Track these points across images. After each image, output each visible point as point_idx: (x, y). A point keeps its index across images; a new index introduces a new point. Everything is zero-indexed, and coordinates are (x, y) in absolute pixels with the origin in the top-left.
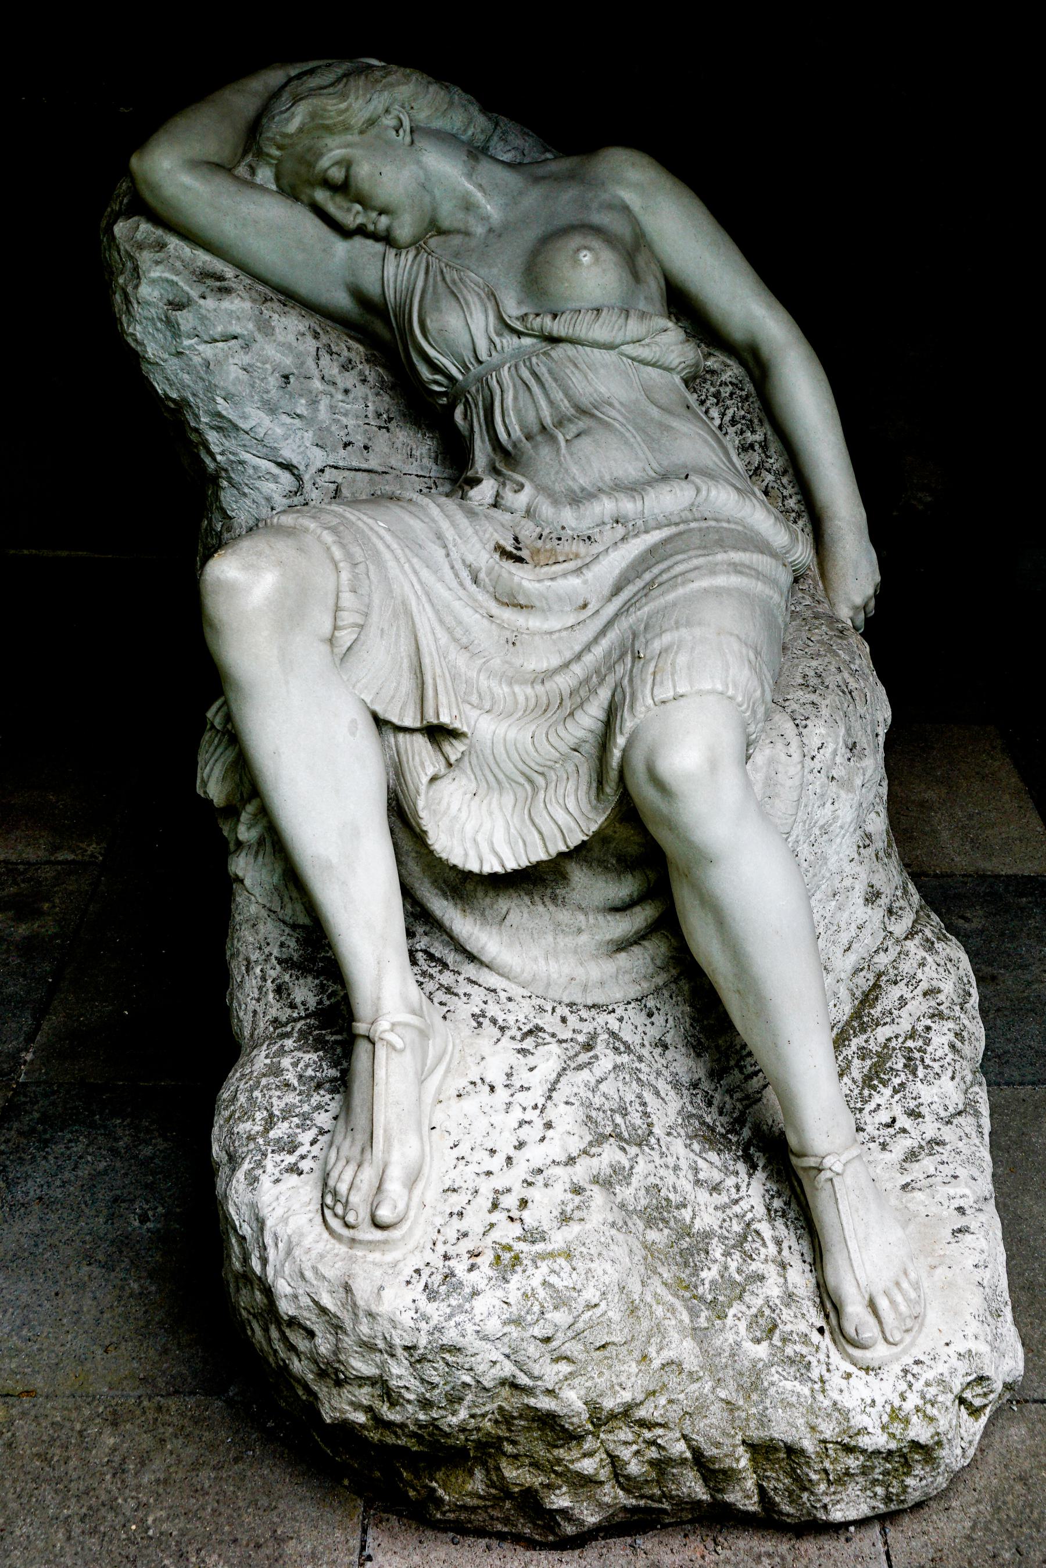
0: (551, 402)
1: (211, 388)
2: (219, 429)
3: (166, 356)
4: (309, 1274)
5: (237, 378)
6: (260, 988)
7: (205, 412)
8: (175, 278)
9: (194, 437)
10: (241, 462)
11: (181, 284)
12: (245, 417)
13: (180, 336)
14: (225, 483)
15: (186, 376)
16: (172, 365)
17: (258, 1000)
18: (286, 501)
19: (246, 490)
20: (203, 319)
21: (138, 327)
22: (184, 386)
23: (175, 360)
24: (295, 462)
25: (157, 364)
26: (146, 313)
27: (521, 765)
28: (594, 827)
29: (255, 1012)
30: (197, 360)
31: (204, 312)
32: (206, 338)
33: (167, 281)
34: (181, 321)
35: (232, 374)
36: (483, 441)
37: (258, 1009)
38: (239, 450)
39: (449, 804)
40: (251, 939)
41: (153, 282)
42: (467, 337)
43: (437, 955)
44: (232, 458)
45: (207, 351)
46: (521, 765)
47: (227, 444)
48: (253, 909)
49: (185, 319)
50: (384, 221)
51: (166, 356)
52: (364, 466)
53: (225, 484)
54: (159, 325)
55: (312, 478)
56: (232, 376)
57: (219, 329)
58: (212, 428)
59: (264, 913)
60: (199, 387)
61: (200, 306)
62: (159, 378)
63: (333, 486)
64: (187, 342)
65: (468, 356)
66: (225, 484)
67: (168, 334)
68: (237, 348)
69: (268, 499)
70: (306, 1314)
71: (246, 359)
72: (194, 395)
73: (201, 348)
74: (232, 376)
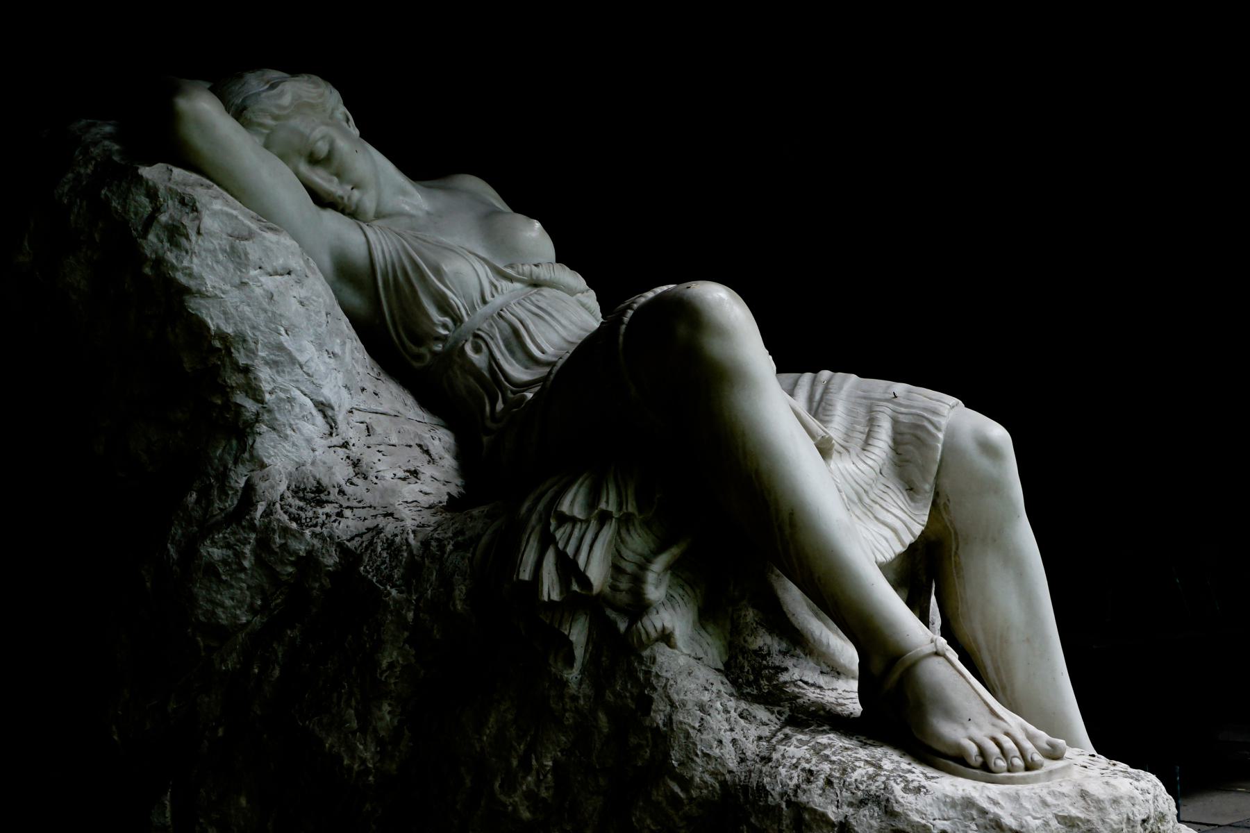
0: (564, 327)
1: (274, 318)
2: (273, 364)
3: (228, 287)
4: (1049, 799)
5: (297, 310)
6: (728, 720)
7: (265, 345)
8: (235, 213)
9: (234, 379)
10: (290, 400)
11: (240, 217)
12: (301, 351)
13: (246, 266)
14: (263, 428)
15: (247, 309)
16: (233, 297)
17: (732, 730)
18: (324, 442)
19: (289, 432)
20: (266, 250)
21: (195, 260)
22: (243, 318)
23: (236, 292)
24: (332, 402)
25: (216, 296)
26: (208, 245)
27: (857, 487)
29: (734, 741)
30: (258, 291)
31: (268, 244)
32: (270, 270)
33: (227, 214)
34: (248, 250)
36: (511, 364)
37: (736, 737)
38: (291, 386)
39: (647, 633)
40: (693, 686)
41: (215, 214)
42: (476, 279)
43: (811, 681)
44: (282, 395)
45: (269, 282)
46: (854, 484)
47: (279, 379)
48: (682, 660)
49: (253, 250)
51: (228, 287)
52: (381, 409)
53: (263, 428)
54: (221, 256)
55: (346, 418)
56: (294, 308)
57: (281, 261)
58: (267, 363)
59: (692, 661)
60: (261, 320)
61: (264, 238)
63: (364, 426)
64: (253, 273)
66: (263, 428)
67: (231, 266)
68: (292, 282)
69: (309, 441)
71: (303, 293)
72: (253, 328)
74: (294, 308)
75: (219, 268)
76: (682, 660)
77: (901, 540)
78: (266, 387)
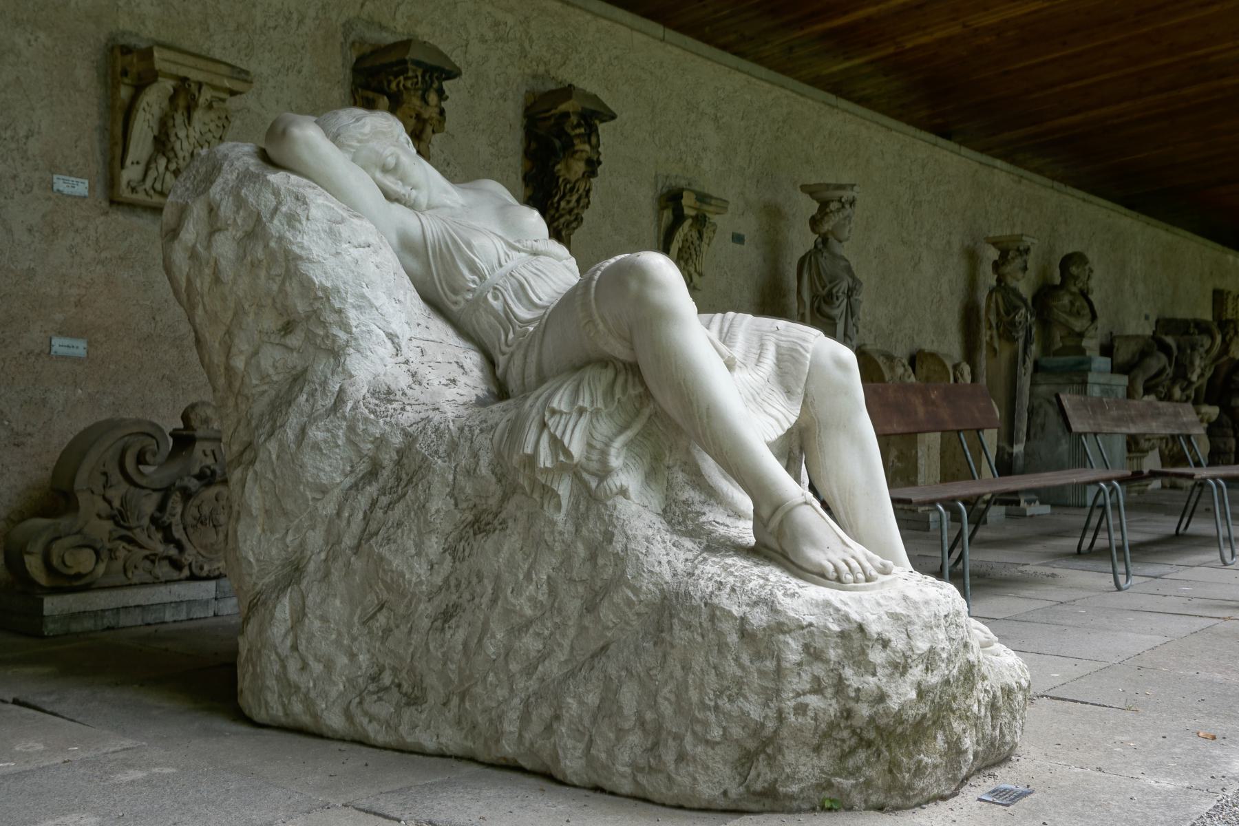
3: (327, 256)
4: (882, 601)
10: (369, 332)
12: (376, 298)
16: (331, 262)
23: (333, 259)
26: (314, 227)
28: (793, 419)
29: (669, 562)
30: (348, 258)
35: (370, 269)
41: (318, 206)
45: (356, 253)
48: (634, 507)
49: (344, 230)
50: (414, 193)
51: (327, 256)
62: (318, 272)
65: (495, 262)
67: (330, 242)
69: (382, 359)
70: (886, 627)
71: (378, 259)
73: (352, 250)
75: (321, 243)
76: (634, 507)
77: (782, 427)
78: (353, 323)
